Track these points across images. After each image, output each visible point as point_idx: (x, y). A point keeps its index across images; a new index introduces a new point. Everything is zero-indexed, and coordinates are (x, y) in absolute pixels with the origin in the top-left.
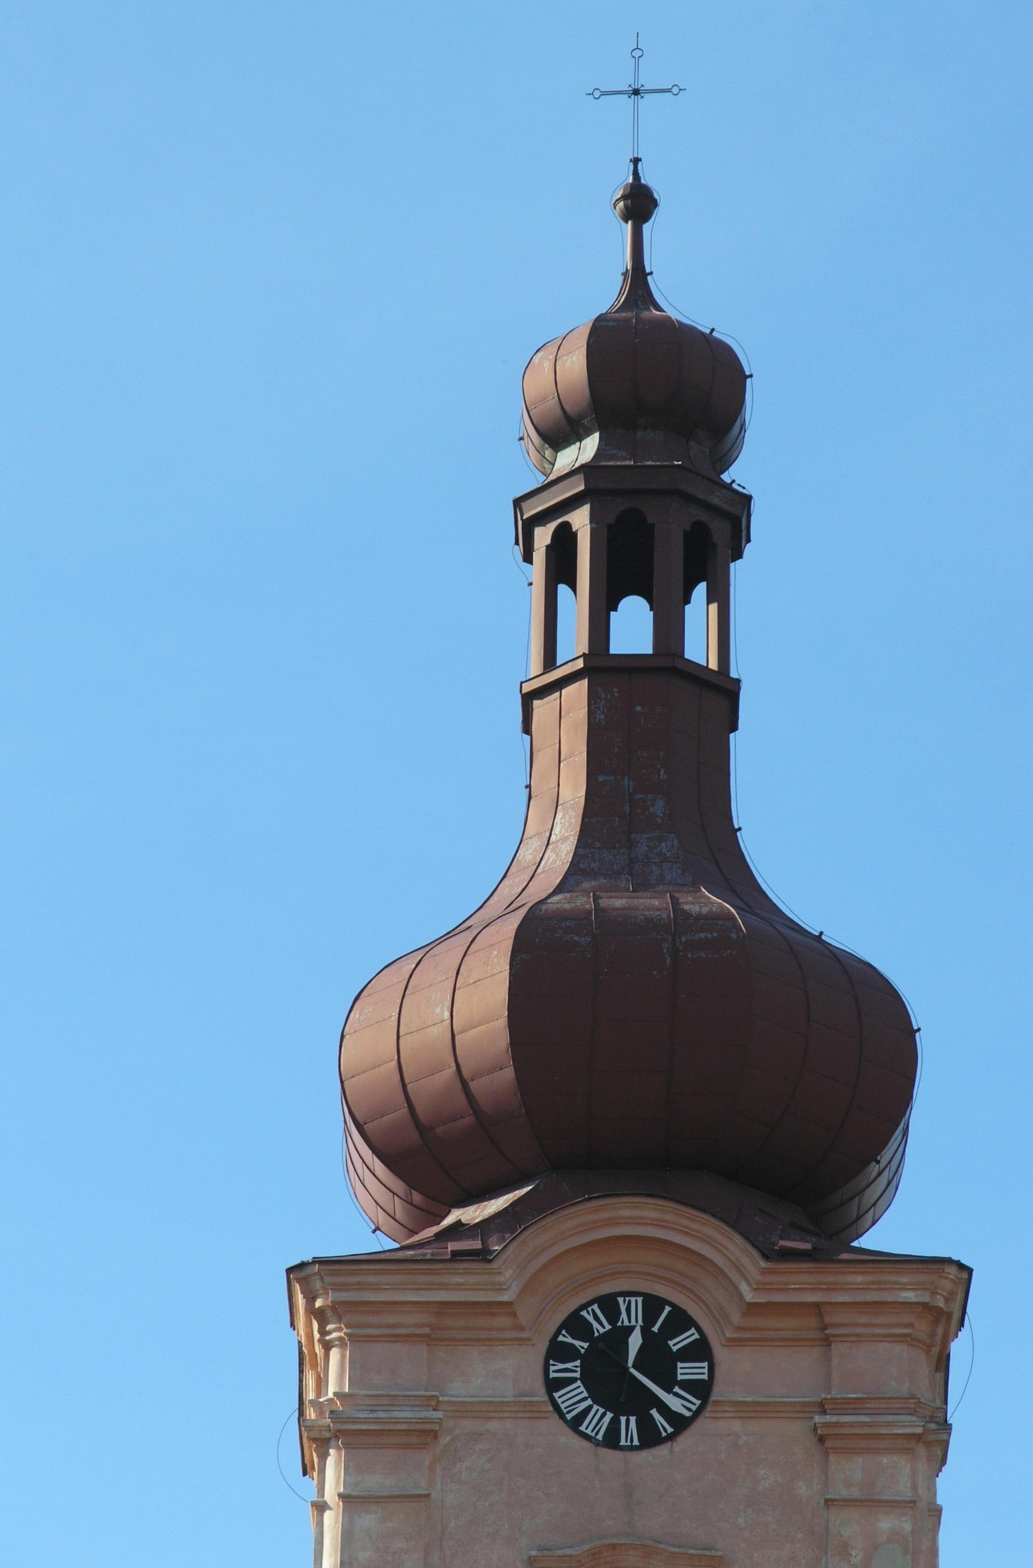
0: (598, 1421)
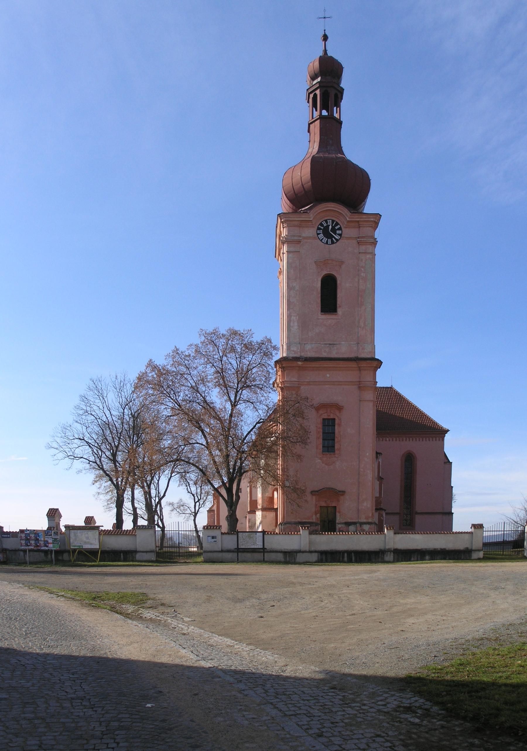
0: (325, 240)
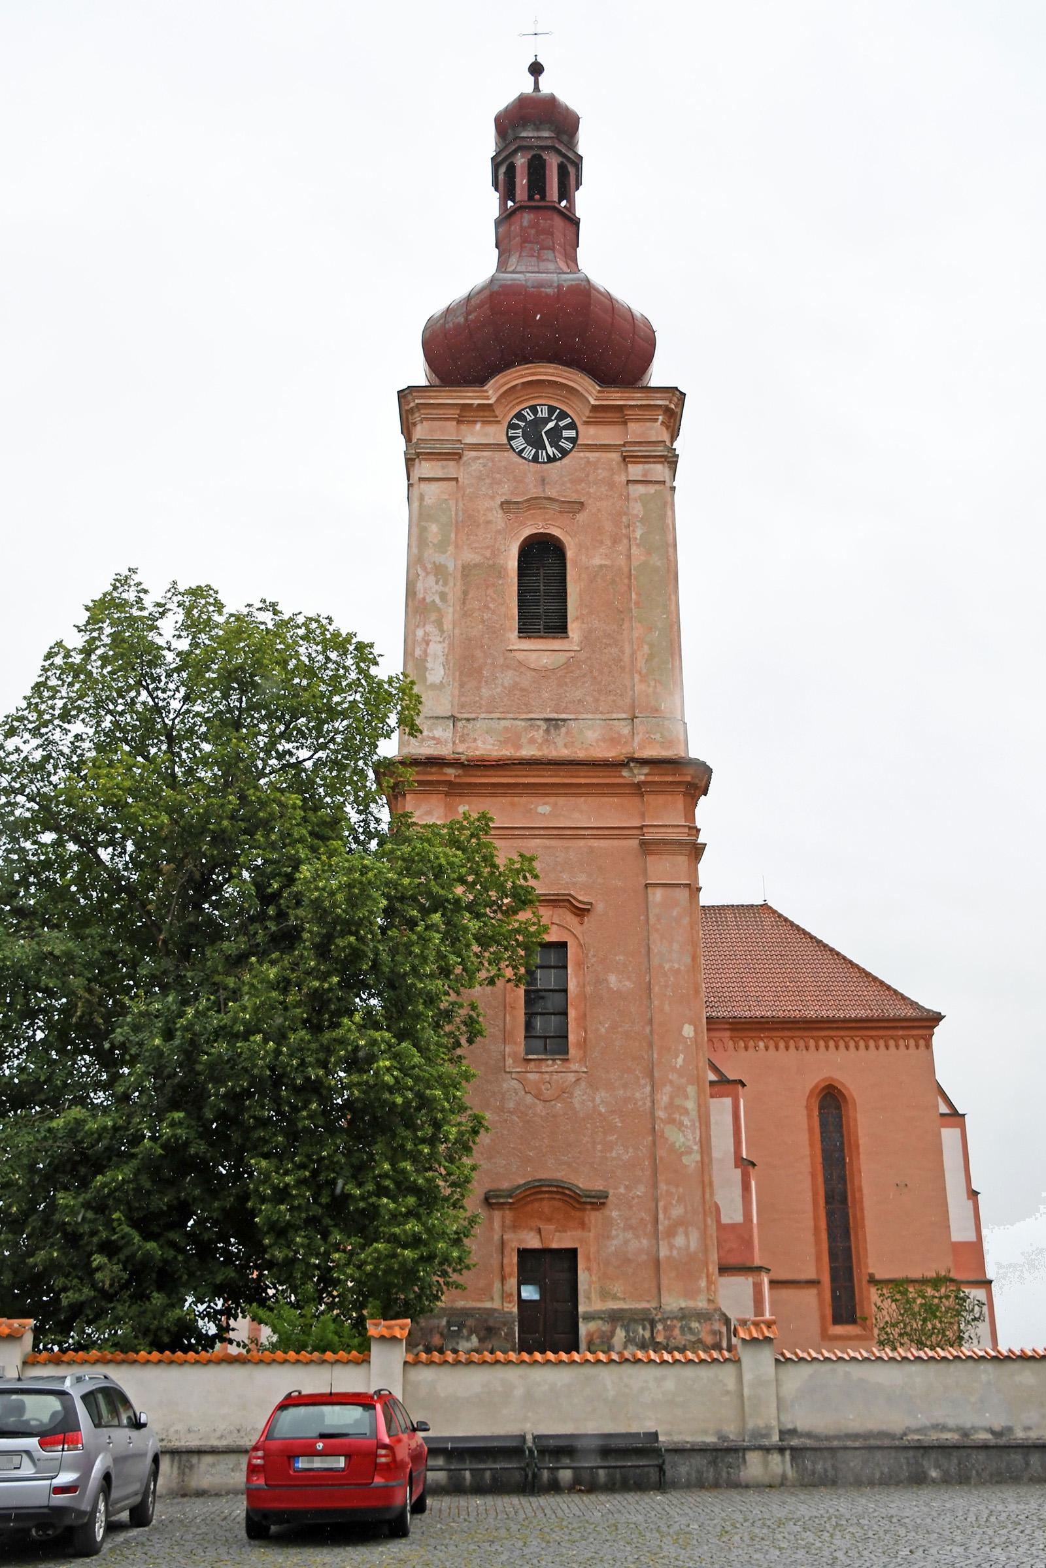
0: (530, 452)
